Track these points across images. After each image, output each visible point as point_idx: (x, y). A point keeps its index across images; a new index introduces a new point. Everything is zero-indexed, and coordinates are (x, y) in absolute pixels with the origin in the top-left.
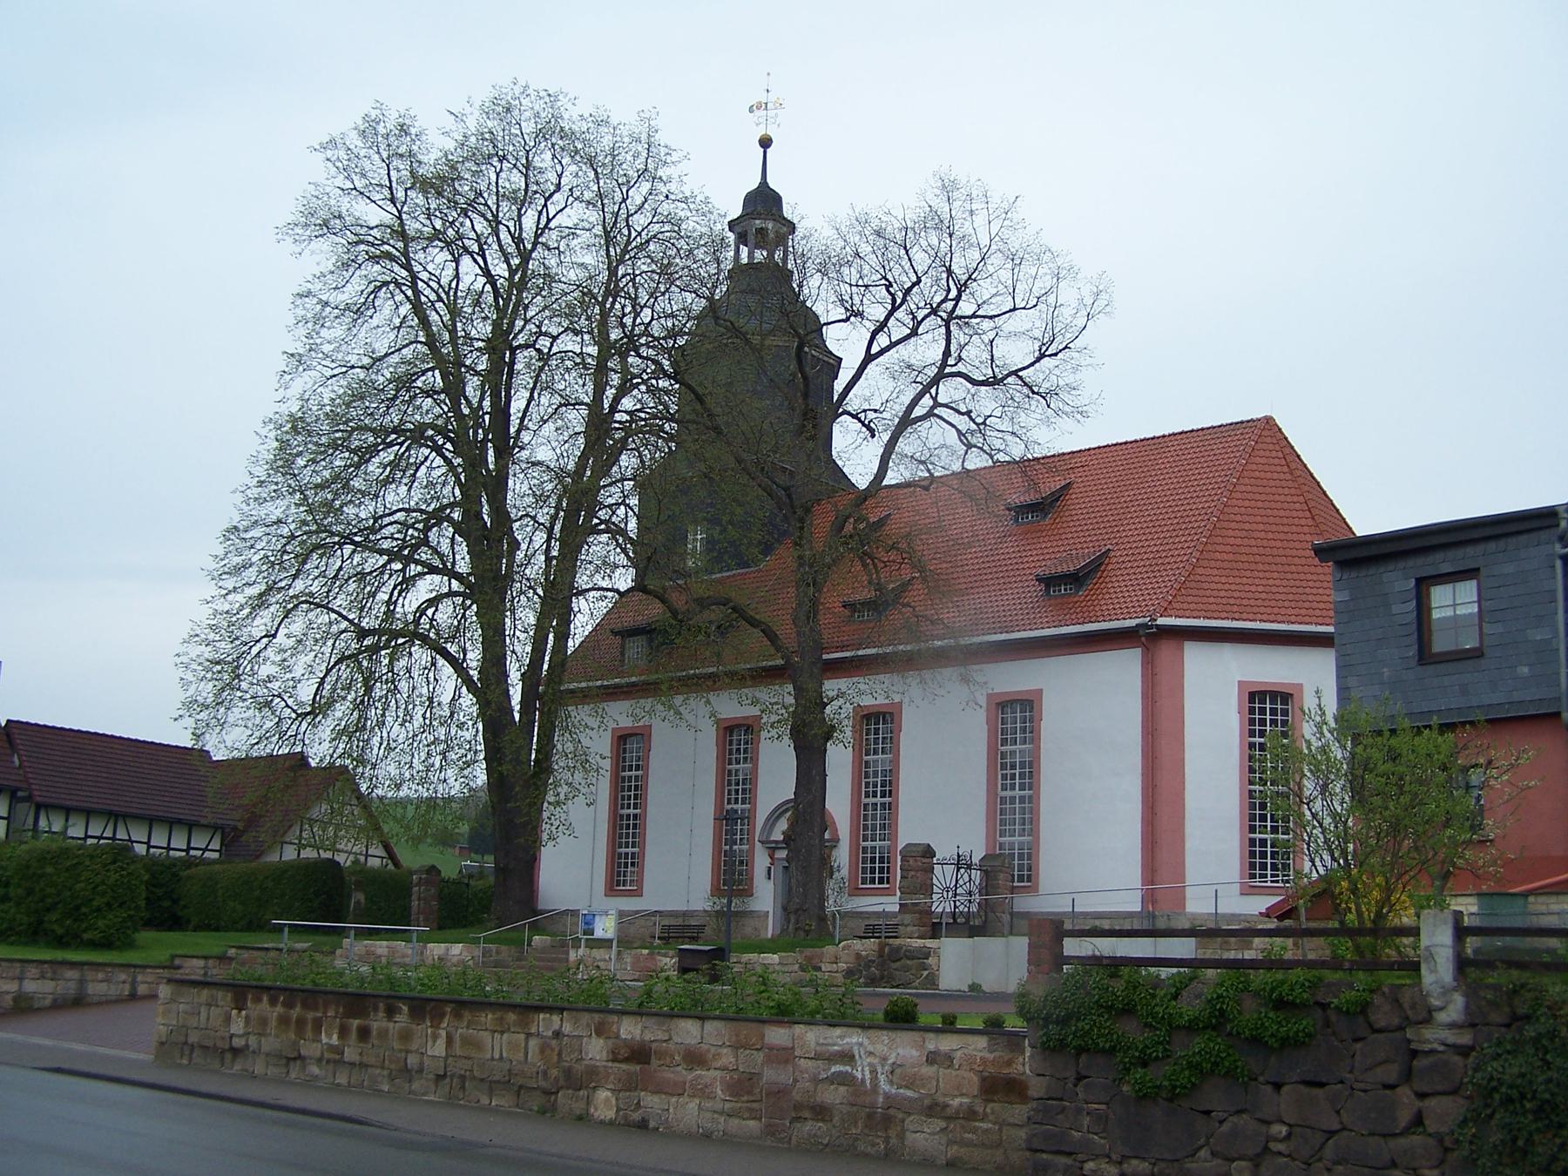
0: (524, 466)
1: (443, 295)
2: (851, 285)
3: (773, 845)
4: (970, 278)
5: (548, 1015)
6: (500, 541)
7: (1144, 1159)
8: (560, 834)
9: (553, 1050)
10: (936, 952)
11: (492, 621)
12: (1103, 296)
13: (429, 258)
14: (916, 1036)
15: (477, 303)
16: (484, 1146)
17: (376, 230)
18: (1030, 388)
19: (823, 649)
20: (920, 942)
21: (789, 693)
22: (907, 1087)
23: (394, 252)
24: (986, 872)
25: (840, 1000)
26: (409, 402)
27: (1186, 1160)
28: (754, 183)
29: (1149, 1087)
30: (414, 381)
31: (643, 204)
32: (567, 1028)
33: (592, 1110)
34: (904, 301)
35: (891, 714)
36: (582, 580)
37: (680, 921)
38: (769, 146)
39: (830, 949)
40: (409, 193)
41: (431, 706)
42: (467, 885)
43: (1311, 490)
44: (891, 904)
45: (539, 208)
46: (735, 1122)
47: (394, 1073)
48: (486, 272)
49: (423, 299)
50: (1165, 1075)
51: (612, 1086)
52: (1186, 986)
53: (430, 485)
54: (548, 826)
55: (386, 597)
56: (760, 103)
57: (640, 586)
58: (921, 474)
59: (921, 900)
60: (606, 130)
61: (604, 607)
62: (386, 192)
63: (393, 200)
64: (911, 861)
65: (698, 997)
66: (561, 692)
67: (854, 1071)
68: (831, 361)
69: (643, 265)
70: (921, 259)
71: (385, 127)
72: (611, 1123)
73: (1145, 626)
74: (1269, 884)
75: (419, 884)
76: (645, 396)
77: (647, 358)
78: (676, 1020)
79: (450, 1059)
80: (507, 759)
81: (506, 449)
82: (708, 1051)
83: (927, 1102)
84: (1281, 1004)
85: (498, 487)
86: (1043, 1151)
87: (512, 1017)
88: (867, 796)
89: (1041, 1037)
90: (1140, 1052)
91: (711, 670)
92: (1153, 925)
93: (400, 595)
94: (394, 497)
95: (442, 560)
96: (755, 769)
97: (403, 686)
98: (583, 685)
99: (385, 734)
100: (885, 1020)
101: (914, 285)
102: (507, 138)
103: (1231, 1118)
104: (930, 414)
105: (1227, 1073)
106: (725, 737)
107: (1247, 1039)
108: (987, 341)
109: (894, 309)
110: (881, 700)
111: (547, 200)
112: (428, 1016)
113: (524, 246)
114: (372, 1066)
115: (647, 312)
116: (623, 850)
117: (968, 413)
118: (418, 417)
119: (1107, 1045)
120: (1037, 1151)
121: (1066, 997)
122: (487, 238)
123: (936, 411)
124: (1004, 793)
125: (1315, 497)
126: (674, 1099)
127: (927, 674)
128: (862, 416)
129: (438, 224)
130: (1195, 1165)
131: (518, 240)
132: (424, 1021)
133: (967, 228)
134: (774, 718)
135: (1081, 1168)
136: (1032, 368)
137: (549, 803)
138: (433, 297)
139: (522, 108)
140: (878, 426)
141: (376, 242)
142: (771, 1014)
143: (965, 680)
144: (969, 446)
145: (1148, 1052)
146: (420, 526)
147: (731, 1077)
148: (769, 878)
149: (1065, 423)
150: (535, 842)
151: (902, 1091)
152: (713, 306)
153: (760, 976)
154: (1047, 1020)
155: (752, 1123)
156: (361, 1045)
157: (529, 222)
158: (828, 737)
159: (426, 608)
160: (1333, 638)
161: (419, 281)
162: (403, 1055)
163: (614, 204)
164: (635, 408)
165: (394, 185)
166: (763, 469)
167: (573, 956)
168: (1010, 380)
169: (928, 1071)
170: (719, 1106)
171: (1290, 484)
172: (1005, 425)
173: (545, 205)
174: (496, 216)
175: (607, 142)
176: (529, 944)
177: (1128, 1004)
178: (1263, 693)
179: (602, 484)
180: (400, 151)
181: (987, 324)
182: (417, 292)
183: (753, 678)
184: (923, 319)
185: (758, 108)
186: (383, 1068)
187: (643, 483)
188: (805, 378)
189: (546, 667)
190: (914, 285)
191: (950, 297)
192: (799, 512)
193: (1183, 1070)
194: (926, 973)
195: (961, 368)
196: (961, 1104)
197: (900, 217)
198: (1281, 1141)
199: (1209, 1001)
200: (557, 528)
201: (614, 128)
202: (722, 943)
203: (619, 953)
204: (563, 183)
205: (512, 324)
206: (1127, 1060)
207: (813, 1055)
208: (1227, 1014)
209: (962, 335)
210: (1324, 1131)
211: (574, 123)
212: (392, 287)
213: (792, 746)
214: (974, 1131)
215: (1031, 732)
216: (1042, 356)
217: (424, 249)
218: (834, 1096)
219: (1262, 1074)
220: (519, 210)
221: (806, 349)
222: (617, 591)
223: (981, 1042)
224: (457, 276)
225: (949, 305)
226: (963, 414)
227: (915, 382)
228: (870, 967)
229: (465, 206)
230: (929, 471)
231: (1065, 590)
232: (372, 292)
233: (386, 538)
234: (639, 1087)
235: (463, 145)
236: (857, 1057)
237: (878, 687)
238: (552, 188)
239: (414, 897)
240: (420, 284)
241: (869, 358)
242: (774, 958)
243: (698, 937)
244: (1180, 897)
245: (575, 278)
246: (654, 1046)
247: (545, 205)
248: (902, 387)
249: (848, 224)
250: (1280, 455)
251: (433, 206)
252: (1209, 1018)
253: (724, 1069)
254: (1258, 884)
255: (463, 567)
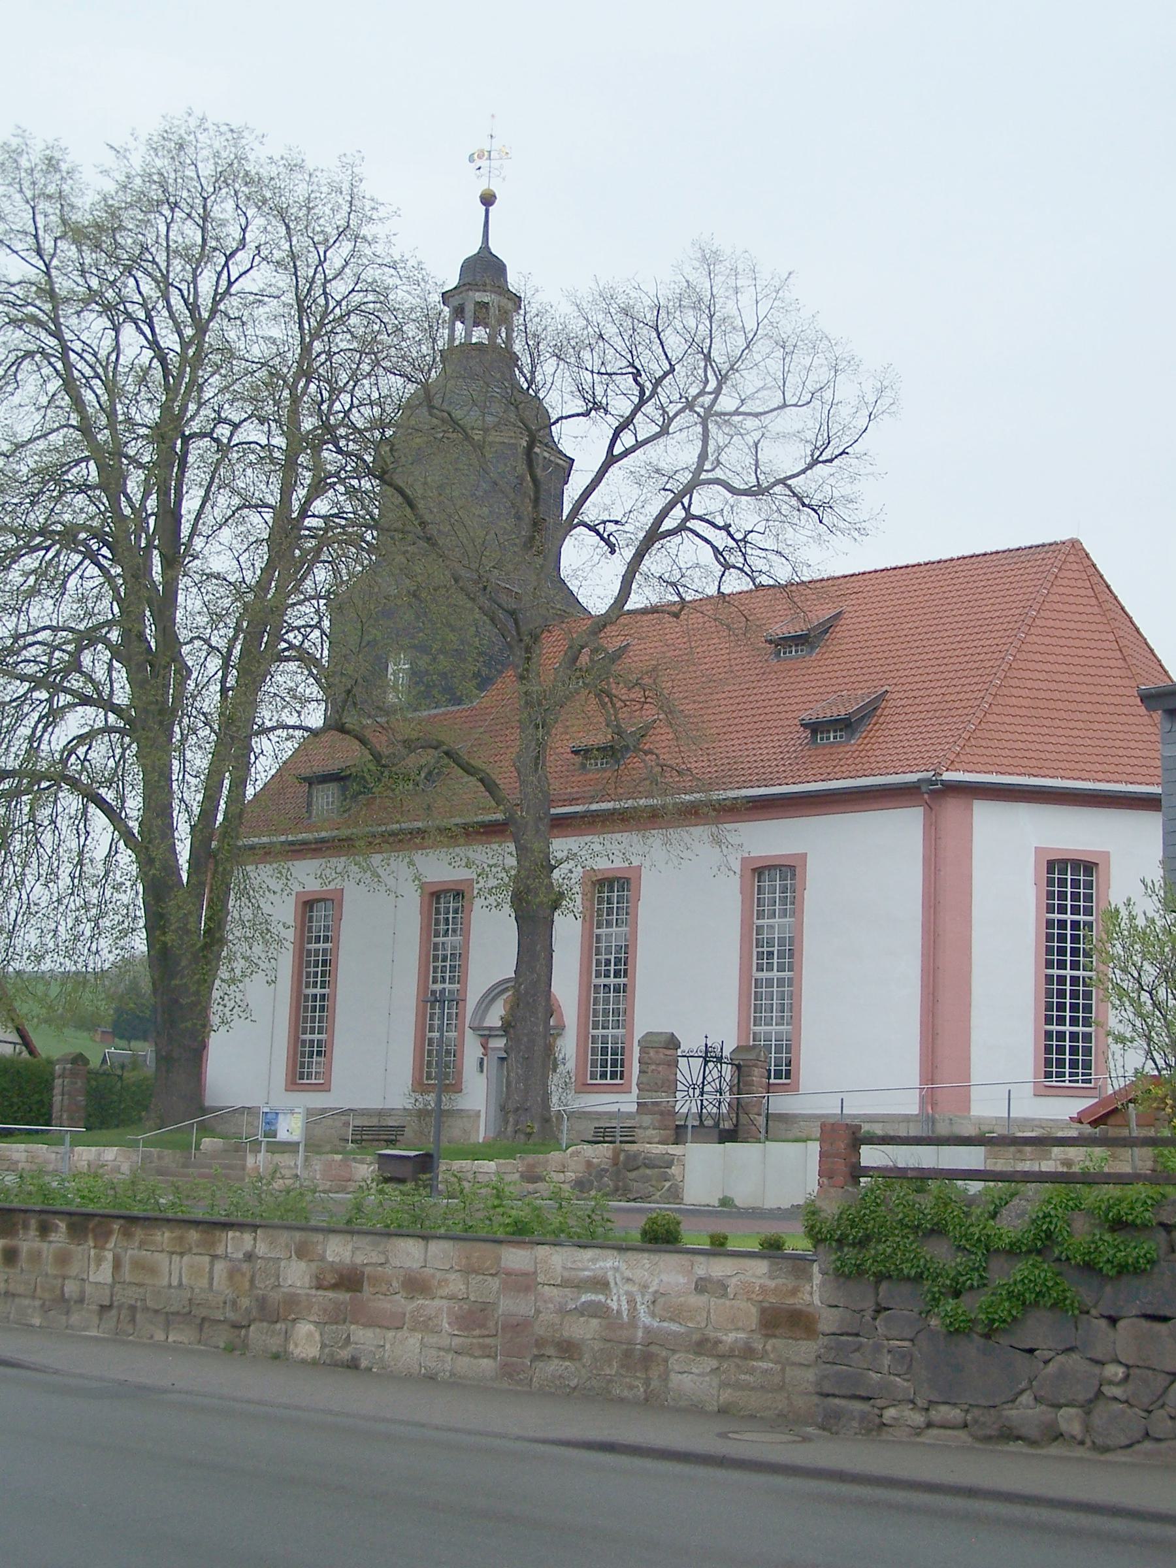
0: (197, 578)
1: (100, 370)
2: (592, 372)
3: (486, 1033)
4: (732, 368)
5: (238, 1234)
6: (168, 666)
7: (955, 1404)
8: (235, 1017)
9: (243, 1275)
10: (681, 1160)
11: (157, 762)
12: (888, 392)
13: (84, 325)
14: (683, 1259)
15: (142, 380)
16: (165, 1391)
17: (18, 287)
18: (800, 499)
19: (551, 803)
20: (660, 1149)
21: (510, 853)
22: (672, 1320)
23: (41, 315)
24: (738, 1067)
25: (589, 1217)
26: (57, 500)
27: (1006, 1406)
28: (473, 249)
29: (962, 1321)
30: (66, 472)
31: (344, 267)
32: (262, 1249)
33: (292, 1347)
34: (654, 393)
35: (628, 880)
36: (266, 715)
37: (374, 1121)
38: (492, 204)
39: (555, 1156)
40: (59, 243)
41: (80, 863)
42: (120, 1077)
43: (1122, 627)
44: (627, 1103)
45: (219, 269)
46: (464, 1361)
47: (47, 1303)
48: (154, 344)
49: (76, 374)
50: (980, 1307)
51: (315, 1318)
52: (1007, 1203)
53: (82, 600)
54: (221, 1008)
55: (28, 732)
56: (482, 151)
57: (335, 725)
58: (671, 598)
59: (662, 1098)
60: (300, 177)
61: (290, 747)
62: (31, 240)
63: (39, 252)
64: (652, 1053)
65: (418, 1211)
66: (239, 848)
67: (609, 1301)
68: (561, 462)
69: (342, 342)
70: (675, 344)
71: (29, 160)
72: (315, 1363)
73: (930, 782)
74: (1067, 1084)
75: (62, 1076)
76: (342, 498)
77: (348, 454)
78: (394, 1240)
79: (118, 1286)
80: (173, 927)
81: (174, 561)
82: (433, 1276)
83: (696, 1337)
84: (1118, 1225)
85: (165, 605)
86: (834, 1396)
87: (194, 1235)
88: (598, 976)
89: (835, 1261)
90: (952, 1280)
91: (420, 824)
92: (933, 1132)
93: (45, 730)
94: (41, 611)
95: (96, 689)
96: (467, 941)
97: (47, 838)
98: (265, 840)
99: (24, 897)
100: (643, 1241)
101: (666, 374)
102: (180, 181)
103: (1059, 1357)
104: (681, 528)
105: (1054, 1305)
106: (430, 905)
107: (1078, 1265)
108: (751, 444)
109: (642, 402)
110: (619, 863)
111: (228, 258)
112: (90, 1235)
113: (200, 314)
114: (20, 1295)
115: (345, 398)
116: (308, 1037)
117: (726, 528)
118: (67, 517)
119: (913, 1272)
120: (828, 1395)
121: (865, 1215)
122: (156, 302)
123: (688, 524)
124: (760, 975)
125: (1126, 635)
126: (390, 1334)
127: (674, 834)
128: (601, 528)
129: (94, 283)
130: (1014, 1412)
131: (193, 308)
132: (86, 1241)
133: (730, 308)
134: (492, 882)
135: (881, 1416)
136: (803, 476)
137: (223, 981)
138: (88, 372)
139: (199, 145)
140: (620, 540)
141: (19, 302)
142: (507, 1233)
143: (718, 841)
144: (727, 566)
145: (962, 1279)
146: (70, 648)
147: (460, 1307)
148: (482, 1071)
149: (840, 542)
150: (204, 1026)
151: (665, 1324)
152: (427, 397)
153: (493, 1188)
154: (840, 1241)
155: (485, 1362)
156: (7, 1270)
157: (206, 285)
158: (556, 906)
159: (77, 746)
160: (1160, 801)
161: (71, 353)
162: (60, 1281)
163: (308, 266)
164: (332, 512)
165: (41, 232)
166: (485, 588)
167: (250, 1161)
168: (778, 489)
169: (696, 1300)
170: (445, 1341)
171: (1098, 619)
172: (770, 544)
173: (226, 264)
174: (165, 277)
175: (301, 191)
176: (197, 1148)
177: (937, 1224)
178: (1065, 862)
179: (290, 602)
180: (47, 192)
181: (751, 423)
182: (68, 366)
183: (468, 835)
184: (676, 415)
185: (480, 157)
186: (33, 1298)
187: (336, 602)
188: (535, 480)
189: (220, 817)
190: (666, 374)
191: (708, 389)
192: (527, 639)
193: (1002, 1300)
194: (667, 1184)
195: (718, 474)
196: (736, 1340)
197: (652, 293)
198: (1118, 1384)
199: (1033, 1221)
200: (236, 652)
201: (310, 175)
202: (430, 1148)
203: (307, 1159)
204: (248, 240)
205: (184, 408)
206: (936, 1289)
207: (559, 1282)
208: (1054, 1236)
209: (720, 435)
210: (1168, 1373)
211: (261, 166)
212: (38, 357)
213: (513, 915)
214: (751, 1371)
215: (793, 903)
216: (815, 462)
217: (78, 313)
218: (585, 1330)
219: (1095, 1306)
220: (195, 270)
221: (537, 450)
222: (306, 729)
223: (761, 1267)
224: (117, 348)
225: (707, 400)
226: (719, 528)
227: (664, 489)
228: (602, 1177)
229: (129, 263)
230: (679, 594)
231: (835, 738)
232: (13, 364)
233: (29, 661)
234: (349, 1318)
235: (125, 187)
236: (612, 1284)
237: (615, 847)
238: (234, 245)
239: (56, 1091)
240: (72, 356)
241: (611, 460)
242: (490, 1166)
243: (396, 1141)
244: (965, 1101)
245: (260, 355)
246: (367, 1270)
247: (226, 264)
248: (649, 495)
249: (590, 299)
250: (1088, 584)
251: (88, 261)
252: (1033, 1240)
253: (451, 1298)
254: (1054, 1084)
255: (122, 698)
